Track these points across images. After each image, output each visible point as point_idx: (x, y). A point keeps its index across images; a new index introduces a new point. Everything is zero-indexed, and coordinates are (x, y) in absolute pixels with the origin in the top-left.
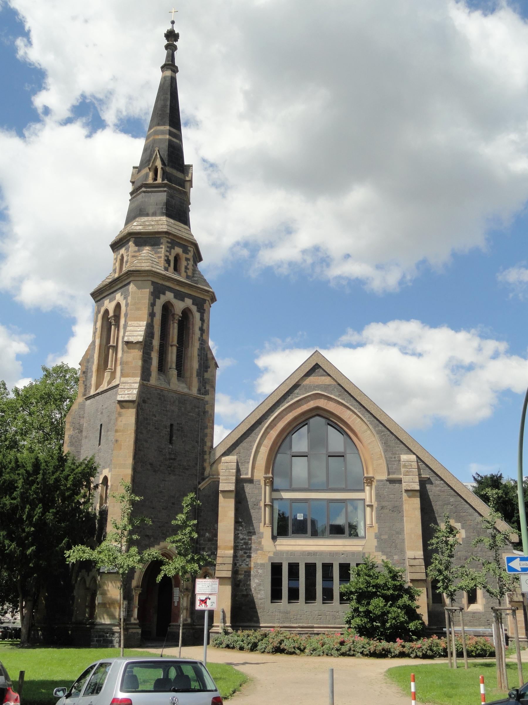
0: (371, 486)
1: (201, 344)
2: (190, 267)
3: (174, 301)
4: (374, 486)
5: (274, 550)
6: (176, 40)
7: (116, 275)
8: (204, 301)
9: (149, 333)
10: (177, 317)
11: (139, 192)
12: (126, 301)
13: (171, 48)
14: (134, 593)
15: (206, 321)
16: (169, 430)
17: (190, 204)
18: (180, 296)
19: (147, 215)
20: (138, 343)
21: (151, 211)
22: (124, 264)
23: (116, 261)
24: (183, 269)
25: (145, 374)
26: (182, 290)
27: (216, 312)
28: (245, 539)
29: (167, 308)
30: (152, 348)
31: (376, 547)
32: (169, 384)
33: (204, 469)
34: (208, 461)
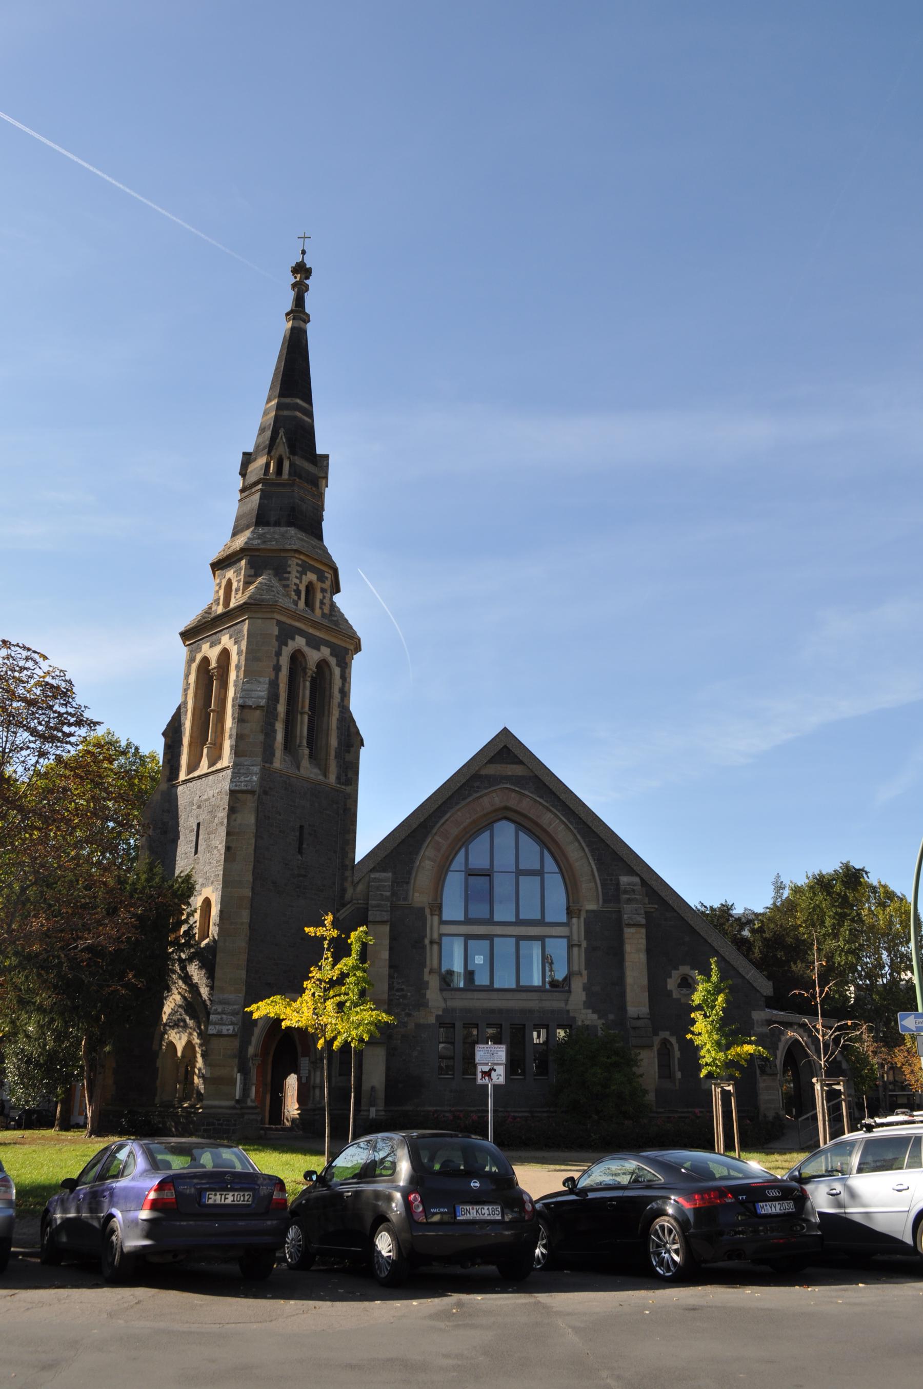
0: (579, 918)
1: (340, 712)
2: (327, 601)
3: (307, 650)
5: (444, 1005)
6: (307, 278)
7: (220, 610)
9: (273, 697)
10: (309, 673)
11: (253, 490)
12: (239, 648)
13: (300, 290)
14: (251, 1065)
16: (298, 834)
17: (323, 510)
18: (314, 643)
20: (258, 707)
21: (273, 519)
22: (233, 593)
23: (220, 587)
24: (318, 604)
26: (317, 634)
27: (358, 663)
28: (402, 990)
29: (297, 658)
31: (585, 1002)
32: (298, 768)
33: (343, 891)
34: (350, 879)
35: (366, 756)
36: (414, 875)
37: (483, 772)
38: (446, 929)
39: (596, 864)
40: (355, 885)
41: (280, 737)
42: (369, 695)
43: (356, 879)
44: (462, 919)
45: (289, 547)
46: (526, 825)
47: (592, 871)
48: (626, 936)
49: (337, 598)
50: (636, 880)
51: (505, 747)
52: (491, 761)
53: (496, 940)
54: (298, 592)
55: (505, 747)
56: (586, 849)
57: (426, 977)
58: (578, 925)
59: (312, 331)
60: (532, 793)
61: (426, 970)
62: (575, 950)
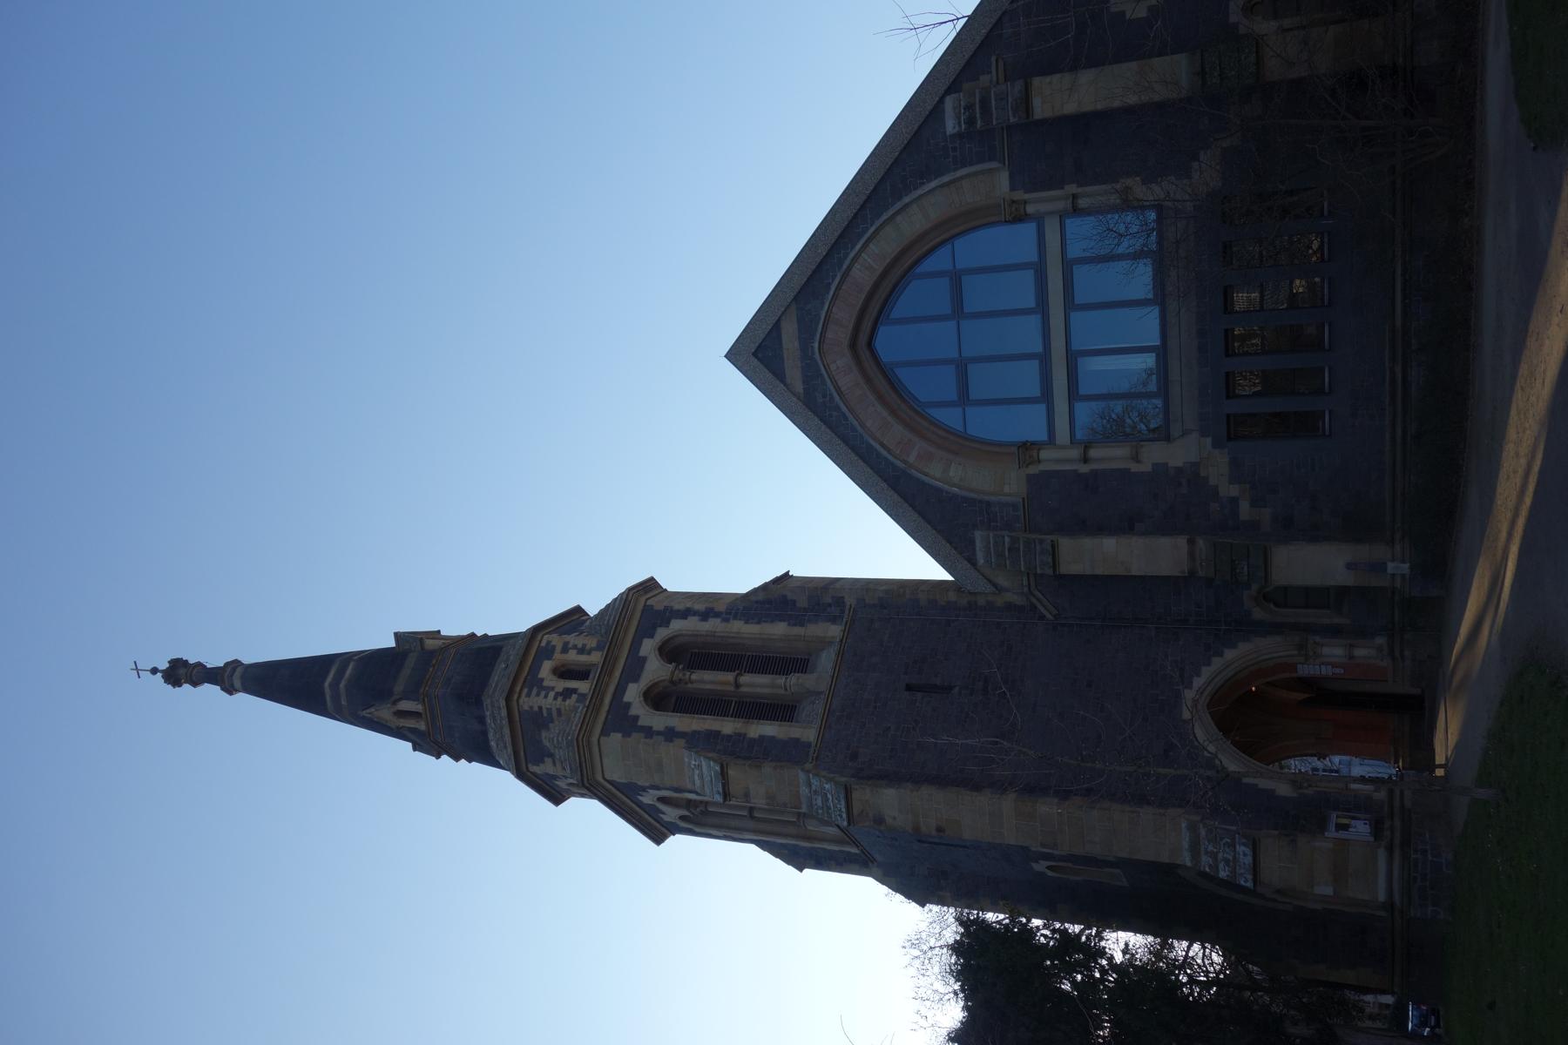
1: (735, 618)
4: (1026, 196)
8: (647, 609)
10: (679, 675)
15: (689, 605)
16: (919, 695)
17: (473, 635)
18: (635, 668)
19: (485, 733)
20: (723, 774)
24: (583, 658)
25: (790, 753)
29: (657, 699)
30: (740, 735)
33: (1010, 607)
35: (804, 568)
36: (973, 495)
37: (799, 387)
38: (1062, 434)
39: (930, 181)
40: (999, 589)
41: (768, 729)
42: (721, 558)
43: (990, 589)
44: (1043, 407)
45: (504, 713)
46: (879, 305)
47: (942, 186)
48: (1048, 114)
49: (593, 610)
50: (949, 103)
51: (755, 354)
52: (780, 375)
53: (1076, 346)
54: (567, 693)
55: (755, 354)
56: (906, 200)
57: (1146, 467)
58: (1041, 202)
59: (253, 655)
60: (823, 303)
61: (1134, 468)
62: (1083, 203)
